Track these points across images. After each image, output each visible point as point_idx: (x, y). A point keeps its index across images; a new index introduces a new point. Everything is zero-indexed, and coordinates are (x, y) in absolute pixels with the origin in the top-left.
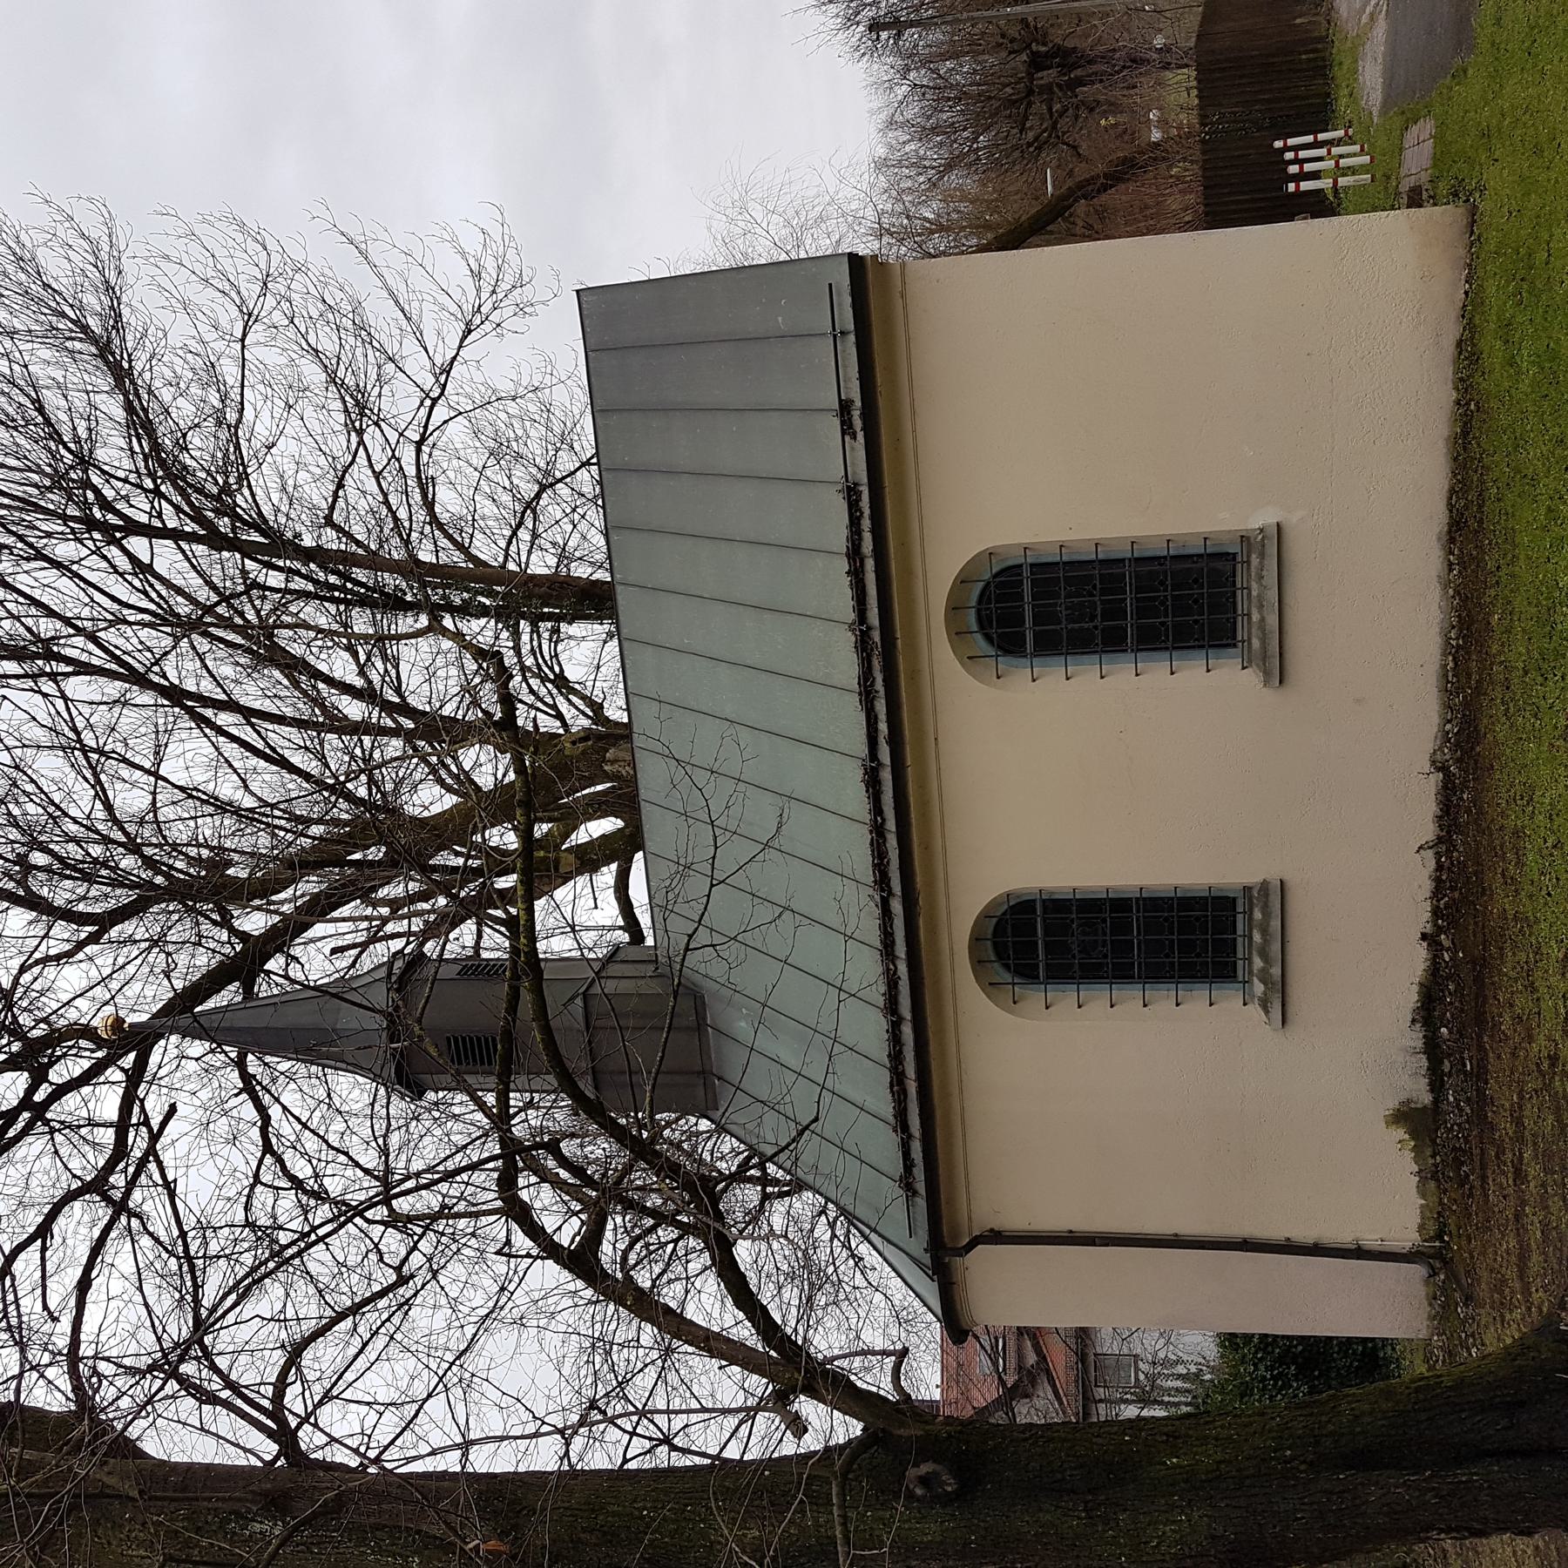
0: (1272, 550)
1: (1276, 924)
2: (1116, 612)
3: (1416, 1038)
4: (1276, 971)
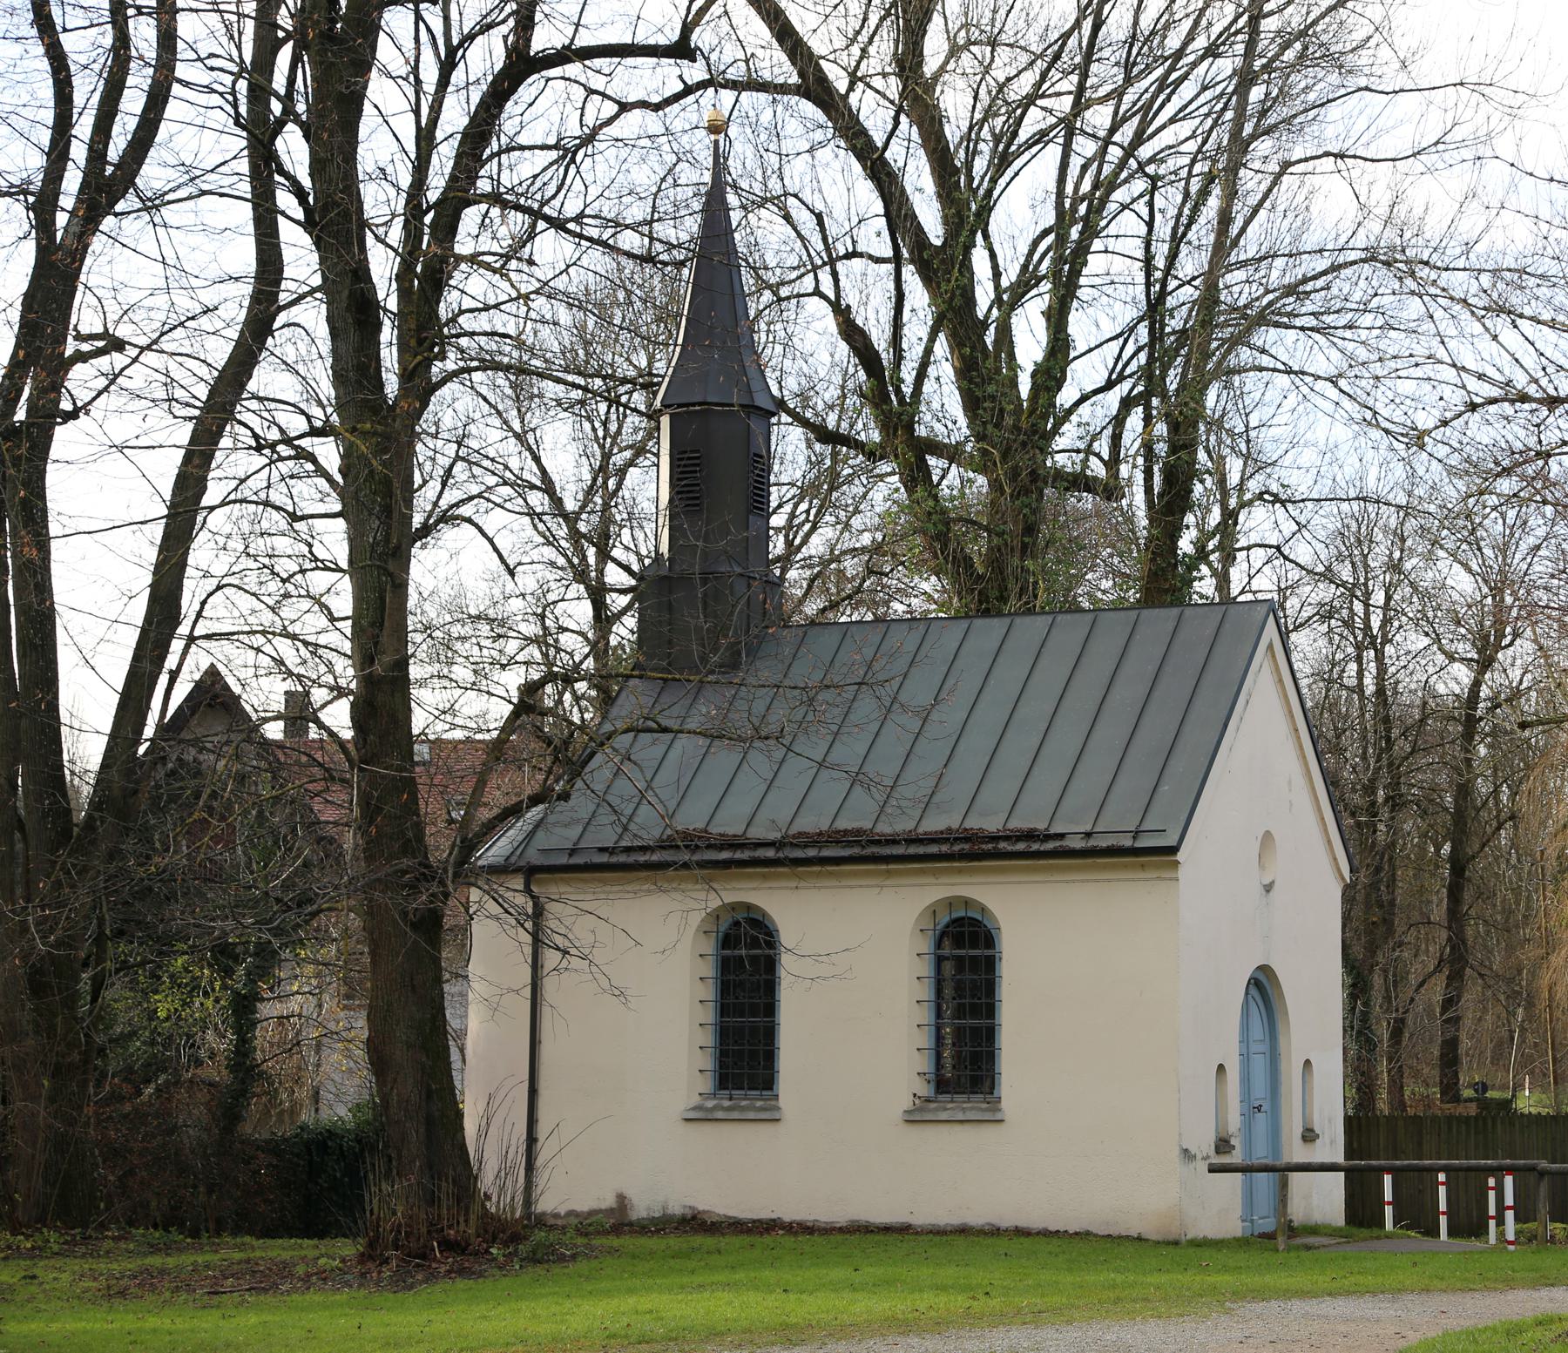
1: (751, 1115)
3: (676, 1209)
4: (720, 1115)
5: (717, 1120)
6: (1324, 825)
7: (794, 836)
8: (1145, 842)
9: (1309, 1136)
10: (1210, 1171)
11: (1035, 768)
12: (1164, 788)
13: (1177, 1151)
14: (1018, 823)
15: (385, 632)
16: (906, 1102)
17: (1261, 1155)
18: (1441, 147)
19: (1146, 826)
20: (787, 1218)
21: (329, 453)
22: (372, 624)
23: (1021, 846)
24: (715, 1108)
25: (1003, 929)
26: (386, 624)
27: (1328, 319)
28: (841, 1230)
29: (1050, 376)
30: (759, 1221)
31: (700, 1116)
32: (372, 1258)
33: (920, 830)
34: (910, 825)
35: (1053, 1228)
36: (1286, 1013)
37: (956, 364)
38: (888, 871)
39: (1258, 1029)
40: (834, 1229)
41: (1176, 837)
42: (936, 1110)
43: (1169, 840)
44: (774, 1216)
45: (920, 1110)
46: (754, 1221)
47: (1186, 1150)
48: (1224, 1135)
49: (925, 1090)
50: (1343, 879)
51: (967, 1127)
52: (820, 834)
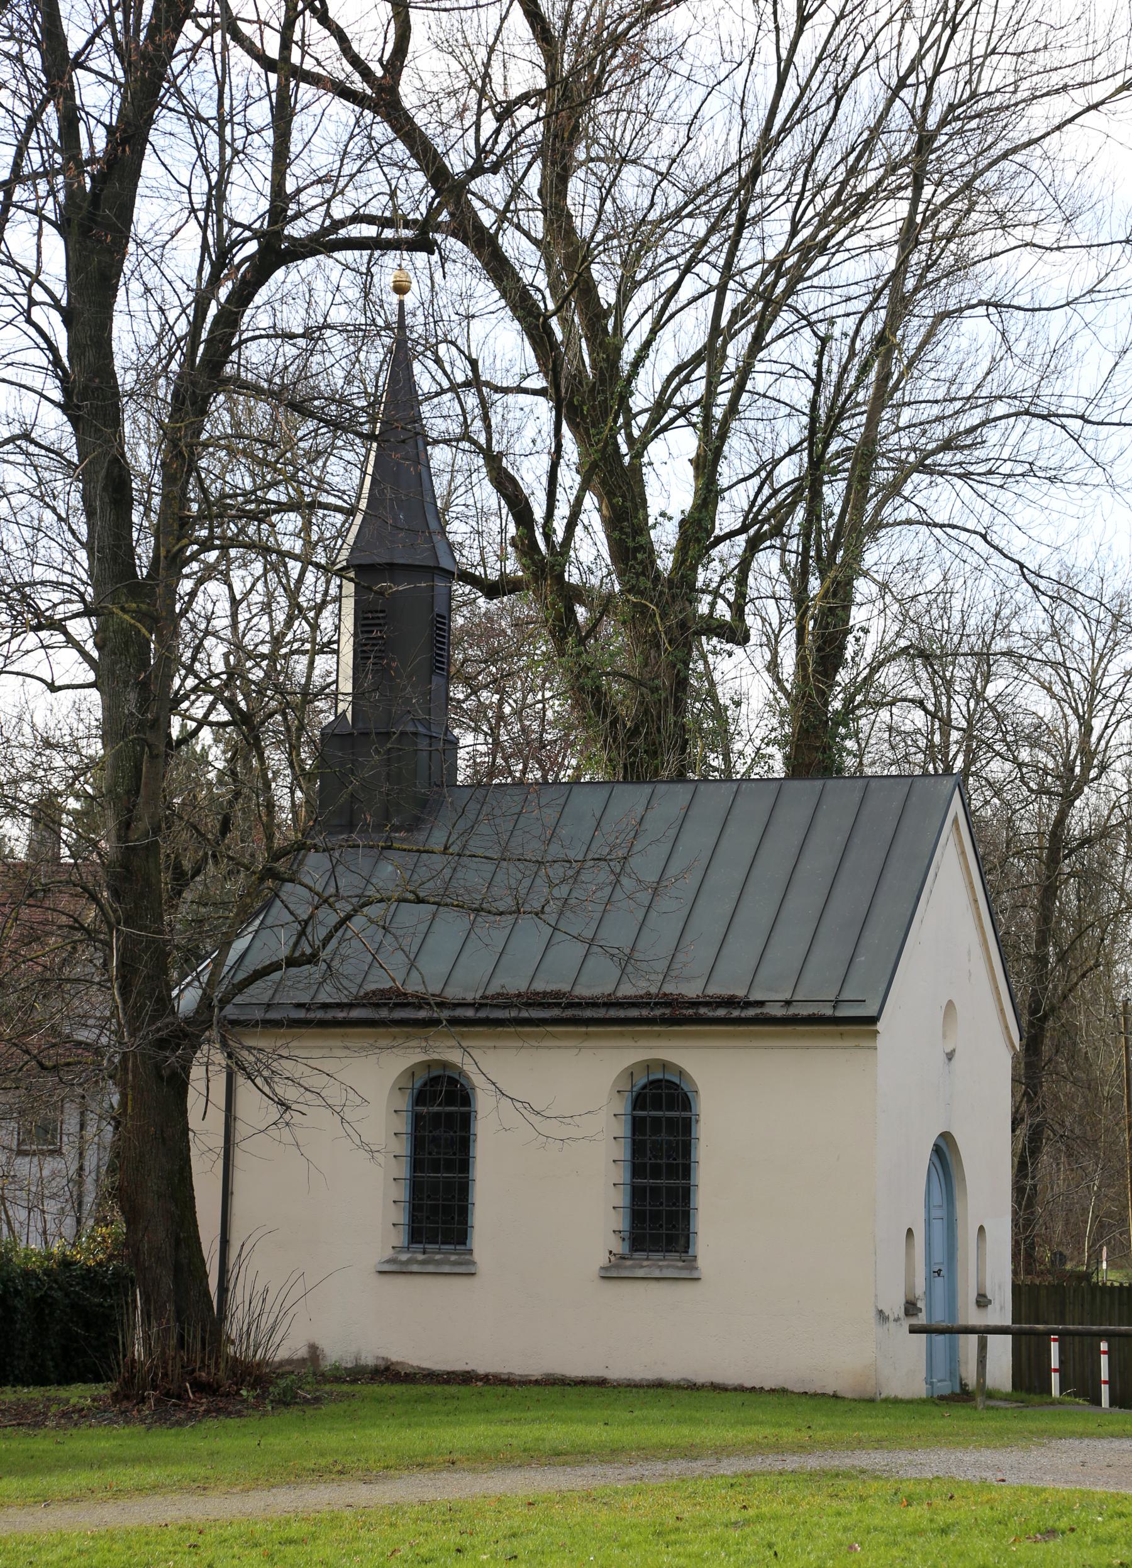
0: (684, 1274)
2: (656, 1172)
4: (415, 1268)
5: (411, 1273)
6: (998, 994)
7: (493, 997)
8: (844, 1012)
9: (982, 1302)
10: (911, 1332)
11: (730, 936)
12: (861, 959)
13: (872, 1314)
14: (716, 990)
15: (140, 800)
16: (603, 1259)
17: (940, 1318)
18: (1095, 296)
19: (843, 997)
20: (481, 1371)
21: (81, 628)
22: (128, 792)
23: (721, 1012)
24: (409, 1262)
25: (701, 1092)
26: (142, 792)
27: (971, 469)
28: (537, 1382)
29: (701, 527)
30: (453, 1373)
31: (393, 1269)
32: (127, 1397)
33: (619, 994)
34: (608, 989)
35: (748, 1385)
36: (964, 1179)
37: (605, 512)
38: (587, 1034)
39: (938, 1197)
40: (530, 1382)
41: (876, 1008)
42: (632, 1267)
43: (869, 1011)
44: (468, 1368)
45: (616, 1267)
46: (448, 1373)
47: (881, 1312)
48: (911, 1298)
49: (620, 1247)
50: (1013, 1047)
51: (663, 1285)
52: (519, 995)
